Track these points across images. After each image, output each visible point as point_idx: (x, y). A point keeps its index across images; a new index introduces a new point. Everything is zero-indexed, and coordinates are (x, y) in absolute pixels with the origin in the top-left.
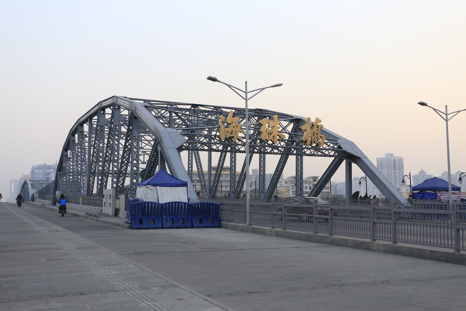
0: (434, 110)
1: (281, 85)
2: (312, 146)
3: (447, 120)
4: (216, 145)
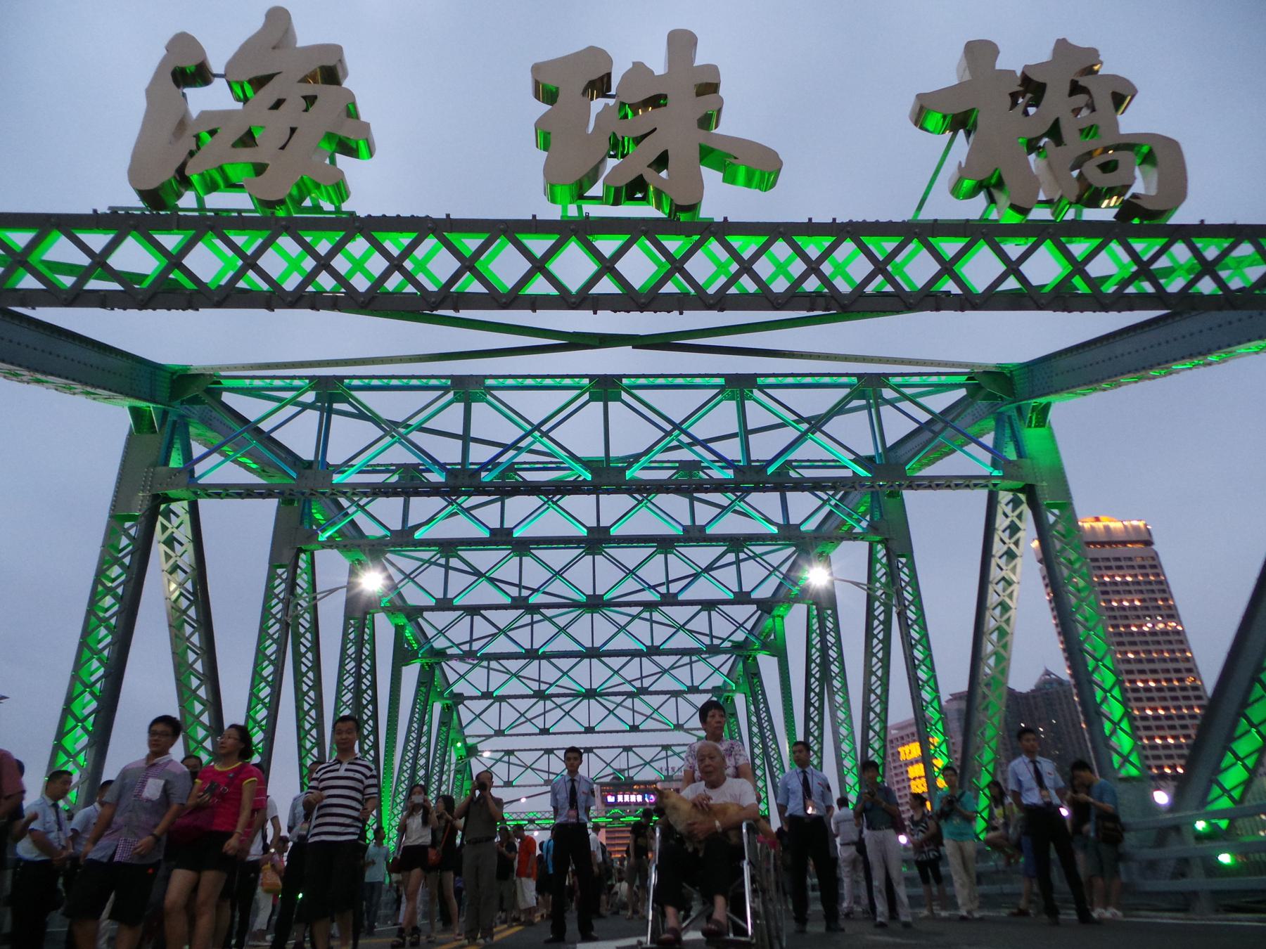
1: (655, 129)
4: (865, 239)
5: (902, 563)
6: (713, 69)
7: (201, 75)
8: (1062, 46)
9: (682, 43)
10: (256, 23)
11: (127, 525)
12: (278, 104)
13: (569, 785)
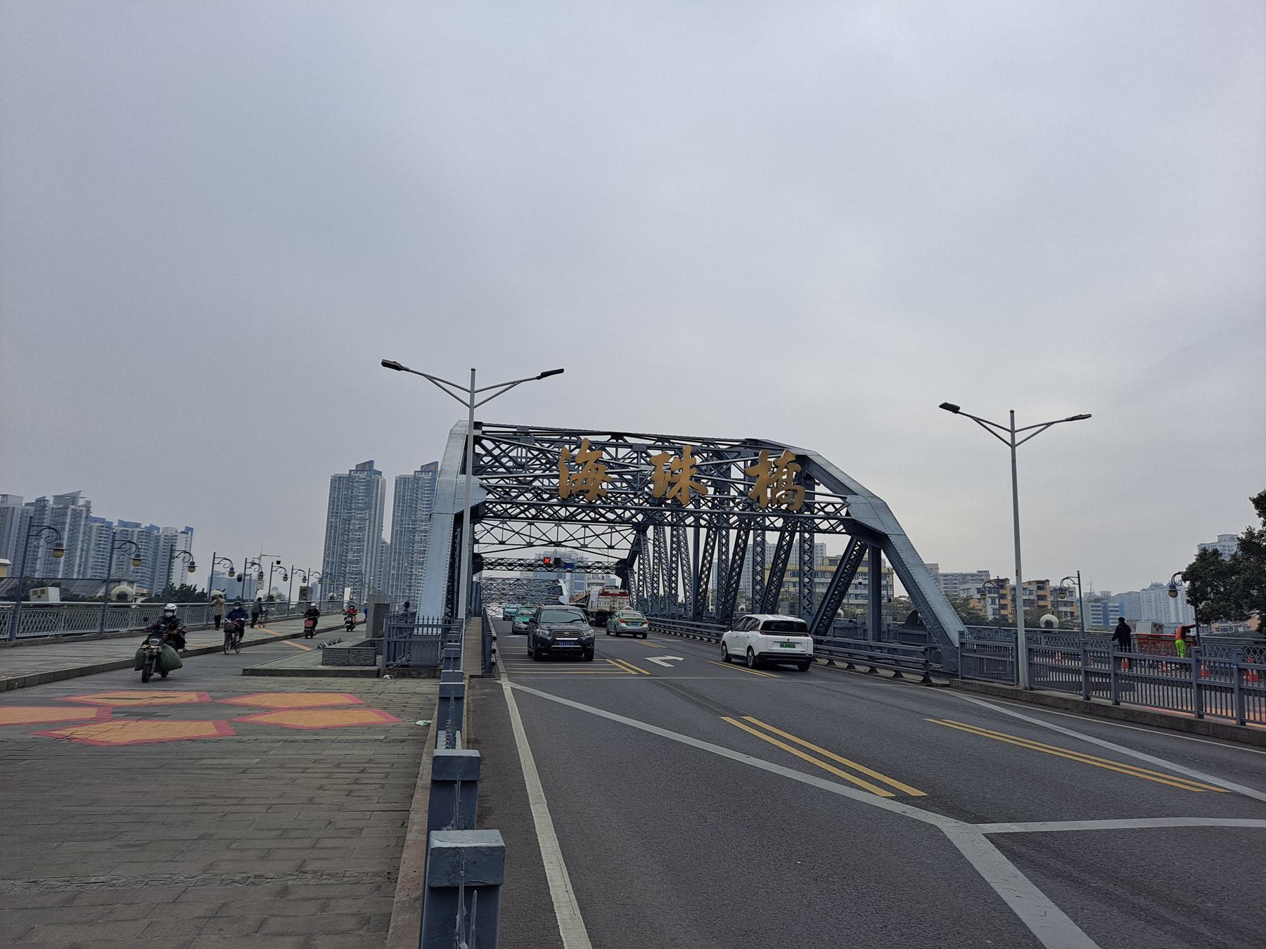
0: (977, 420)
1: (1090, 416)
2: (825, 512)
3: (1013, 446)
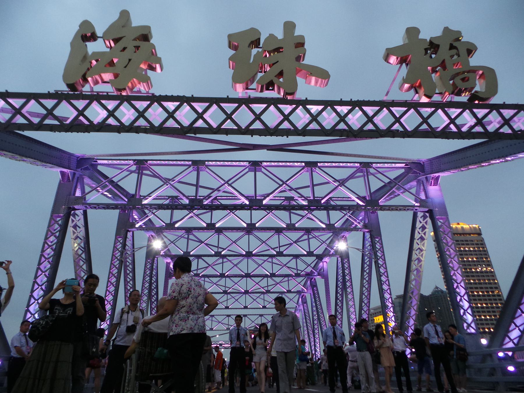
1: (278, 61)
5: (376, 241)
6: (302, 37)
7: (93, 37)
8: (446, 29)
9: (289, 26)
10: (115, 17)
11: (58, 219)
12: (124, 49)
13: (237, 331)
